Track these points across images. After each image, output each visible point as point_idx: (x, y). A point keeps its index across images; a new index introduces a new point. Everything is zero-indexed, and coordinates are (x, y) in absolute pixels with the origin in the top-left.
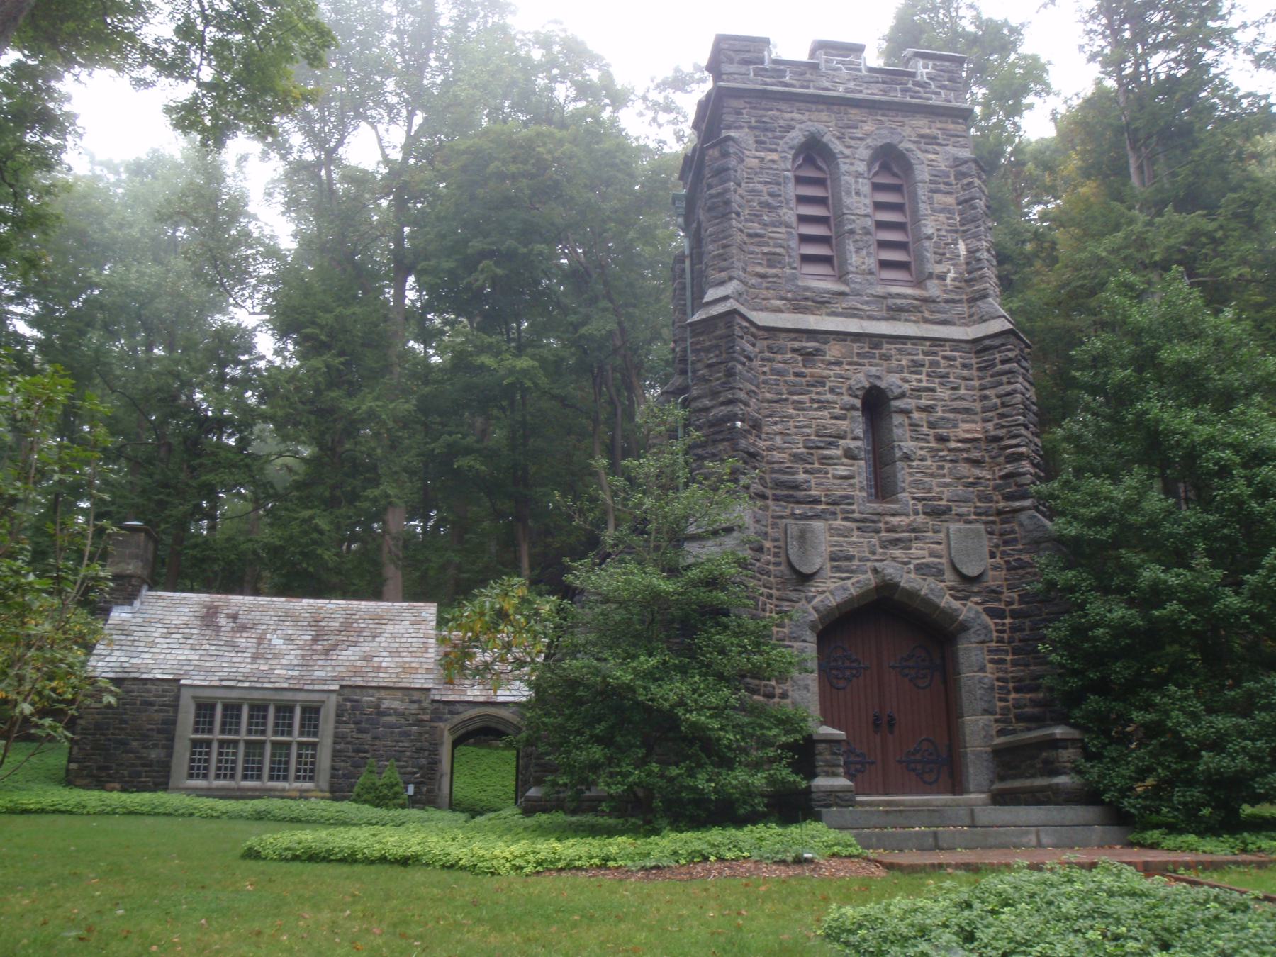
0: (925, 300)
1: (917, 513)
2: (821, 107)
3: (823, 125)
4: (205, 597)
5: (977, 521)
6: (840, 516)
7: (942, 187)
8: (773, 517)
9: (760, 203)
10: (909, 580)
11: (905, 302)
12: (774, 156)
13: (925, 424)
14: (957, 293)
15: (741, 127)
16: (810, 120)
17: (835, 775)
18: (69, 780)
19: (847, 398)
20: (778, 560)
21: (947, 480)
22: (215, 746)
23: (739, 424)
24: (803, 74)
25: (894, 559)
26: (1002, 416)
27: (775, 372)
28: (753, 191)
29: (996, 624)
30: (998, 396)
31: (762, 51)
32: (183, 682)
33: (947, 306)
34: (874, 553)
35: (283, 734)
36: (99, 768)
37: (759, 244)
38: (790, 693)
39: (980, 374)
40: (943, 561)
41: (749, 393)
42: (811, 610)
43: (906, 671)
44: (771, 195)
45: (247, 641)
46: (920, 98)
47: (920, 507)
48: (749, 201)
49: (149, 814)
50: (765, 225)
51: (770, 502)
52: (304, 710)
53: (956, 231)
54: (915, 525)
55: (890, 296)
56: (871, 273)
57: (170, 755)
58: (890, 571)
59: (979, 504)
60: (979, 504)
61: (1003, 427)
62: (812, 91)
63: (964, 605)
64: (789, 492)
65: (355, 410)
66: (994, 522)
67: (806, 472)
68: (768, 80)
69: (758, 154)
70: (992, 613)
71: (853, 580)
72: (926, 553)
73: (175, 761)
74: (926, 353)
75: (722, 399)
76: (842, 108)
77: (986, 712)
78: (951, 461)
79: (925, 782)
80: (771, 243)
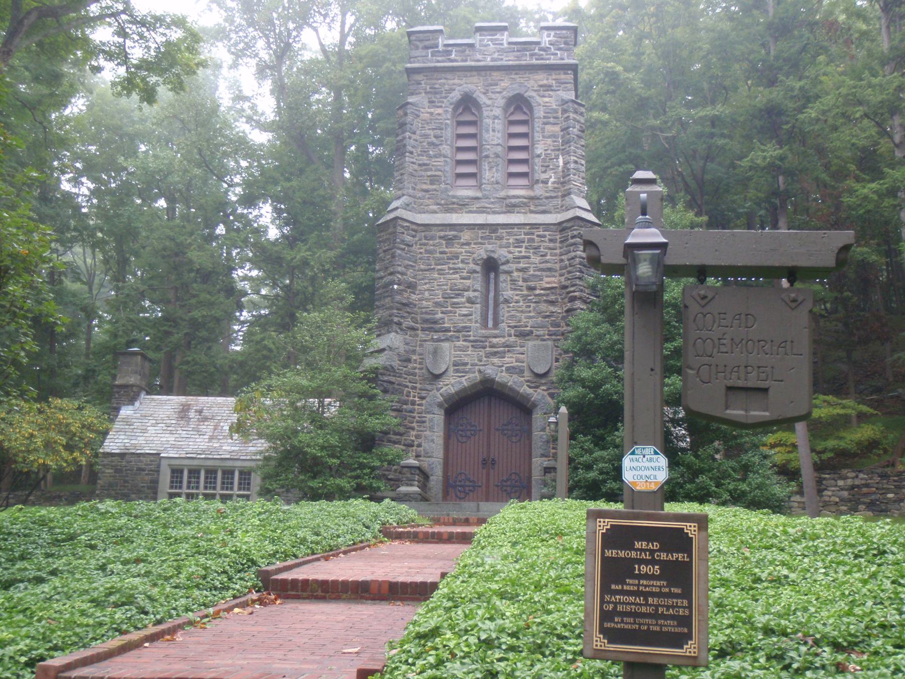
0: (532, 198)
1: (510, 336)
3: (474, 85)
4: (182, 399)
5: (548, 339)
7: (552, 120)
10: (502, 377)
11: (517, 200)
12: (440, 111)
15: (420, 93)
17: (412, 485)
19: (472, 266)
21: (532, 314)
23: (396, 287)
25: (493, 364)
26: (569, 272)
27: (427, 252)
28: (425, 135)
33: (547, 201)
34: (481, 361)
35: (227, 489)
37: (426, 170)
41: (407, 267)
44: (436, 137)
45: (207, 428)
46: (542, 59)
47: (512, 332)
51: (419, 332)
52: (241, 473)
53: (558, 150)
55: (508, 197)
62: (468, 63)
64: (431, 325)
65: (292, 259)
67: (442, 313)
68: (440, 59)
69: (429, 110)
72: (514, 360)
74: (526, 234)
76: (488, 73)
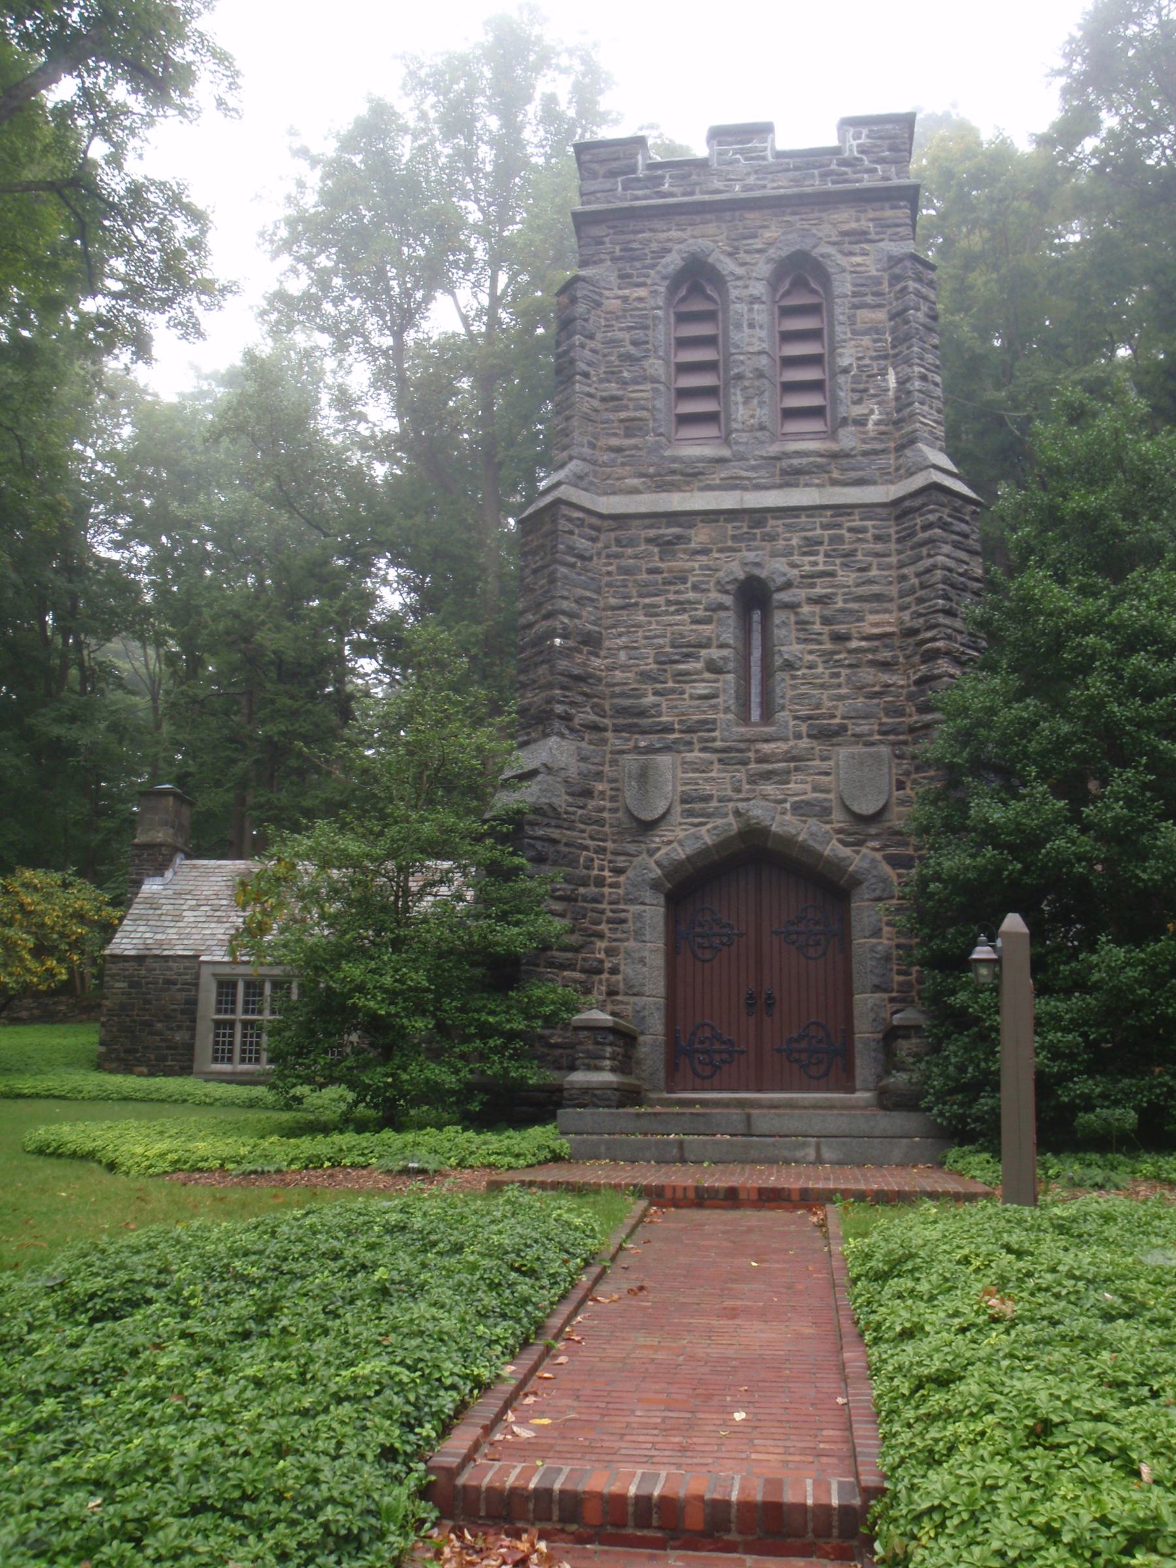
0: (834, 456)
1: (798, 736)
2: (708, 216)
5: (881, 742)
6: (697, 746)
7: (869, 299)
8: (612, 752)
9: (620, 356)
10: (784, 823)
11: (804, 461)
12: (642, 292)
13: (818, 620)
14: (881, 441)
15: (602, 261)
16: (694, 237)
17: (598, 1069)
18: (101, 1064)
19: (715, 596)
20: (615, 805)
21: (844, 691)
22: (238, 1028)
23: (558, 641)
24: (684, 177)
25: (765, 797)
26: (920, 601)
28: (612, 341)
29: (900, 876)
30: (918, 575)
31: (634, 156)
32: (202, 958)
33: (865, 460)
34: (738, 791)
36: (127, 1051)
37: (616, 410)
38: (622, 968)
39: (899, 547)
40: (831, 796)
41: (579, 601)
42: (654, 865)
43: (794, 937)
44: (635, 343)
47: (804, 728)
48: (605, 356)
49: (142, 1100)
50: (625, 383)
51: (609, 735)
53: (885, 357)
54: (795, 752)
56: (762, 428)
57: (193, 1037)
58: (757, 812)
59: (885, 720)
60: (885, 720)
61: (921, 615)
62: (698, 197)
63: (857, 852)
66: (905, 743)
68: (640, 193)
69: (621, 293)
70: (893, 861)
71: (709, 826)
72: (808, 787)
73: (198, 1044)
74: (824, 527)
75: (544, 612)
76: (737, 214)
77: (877, 988)
78: (850, 666)
79: (811, 1077)
80: (631, 405)
